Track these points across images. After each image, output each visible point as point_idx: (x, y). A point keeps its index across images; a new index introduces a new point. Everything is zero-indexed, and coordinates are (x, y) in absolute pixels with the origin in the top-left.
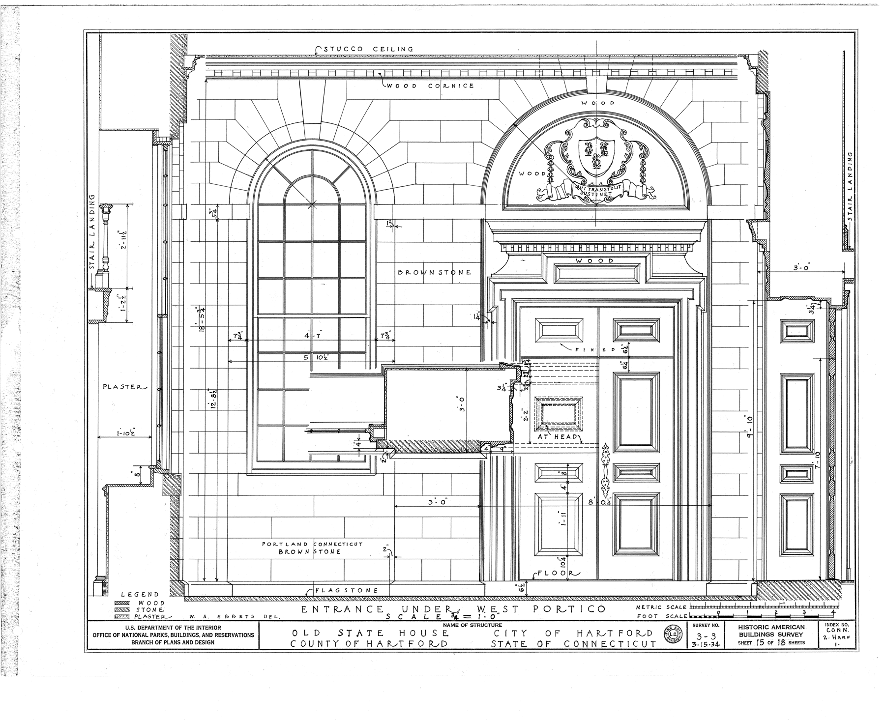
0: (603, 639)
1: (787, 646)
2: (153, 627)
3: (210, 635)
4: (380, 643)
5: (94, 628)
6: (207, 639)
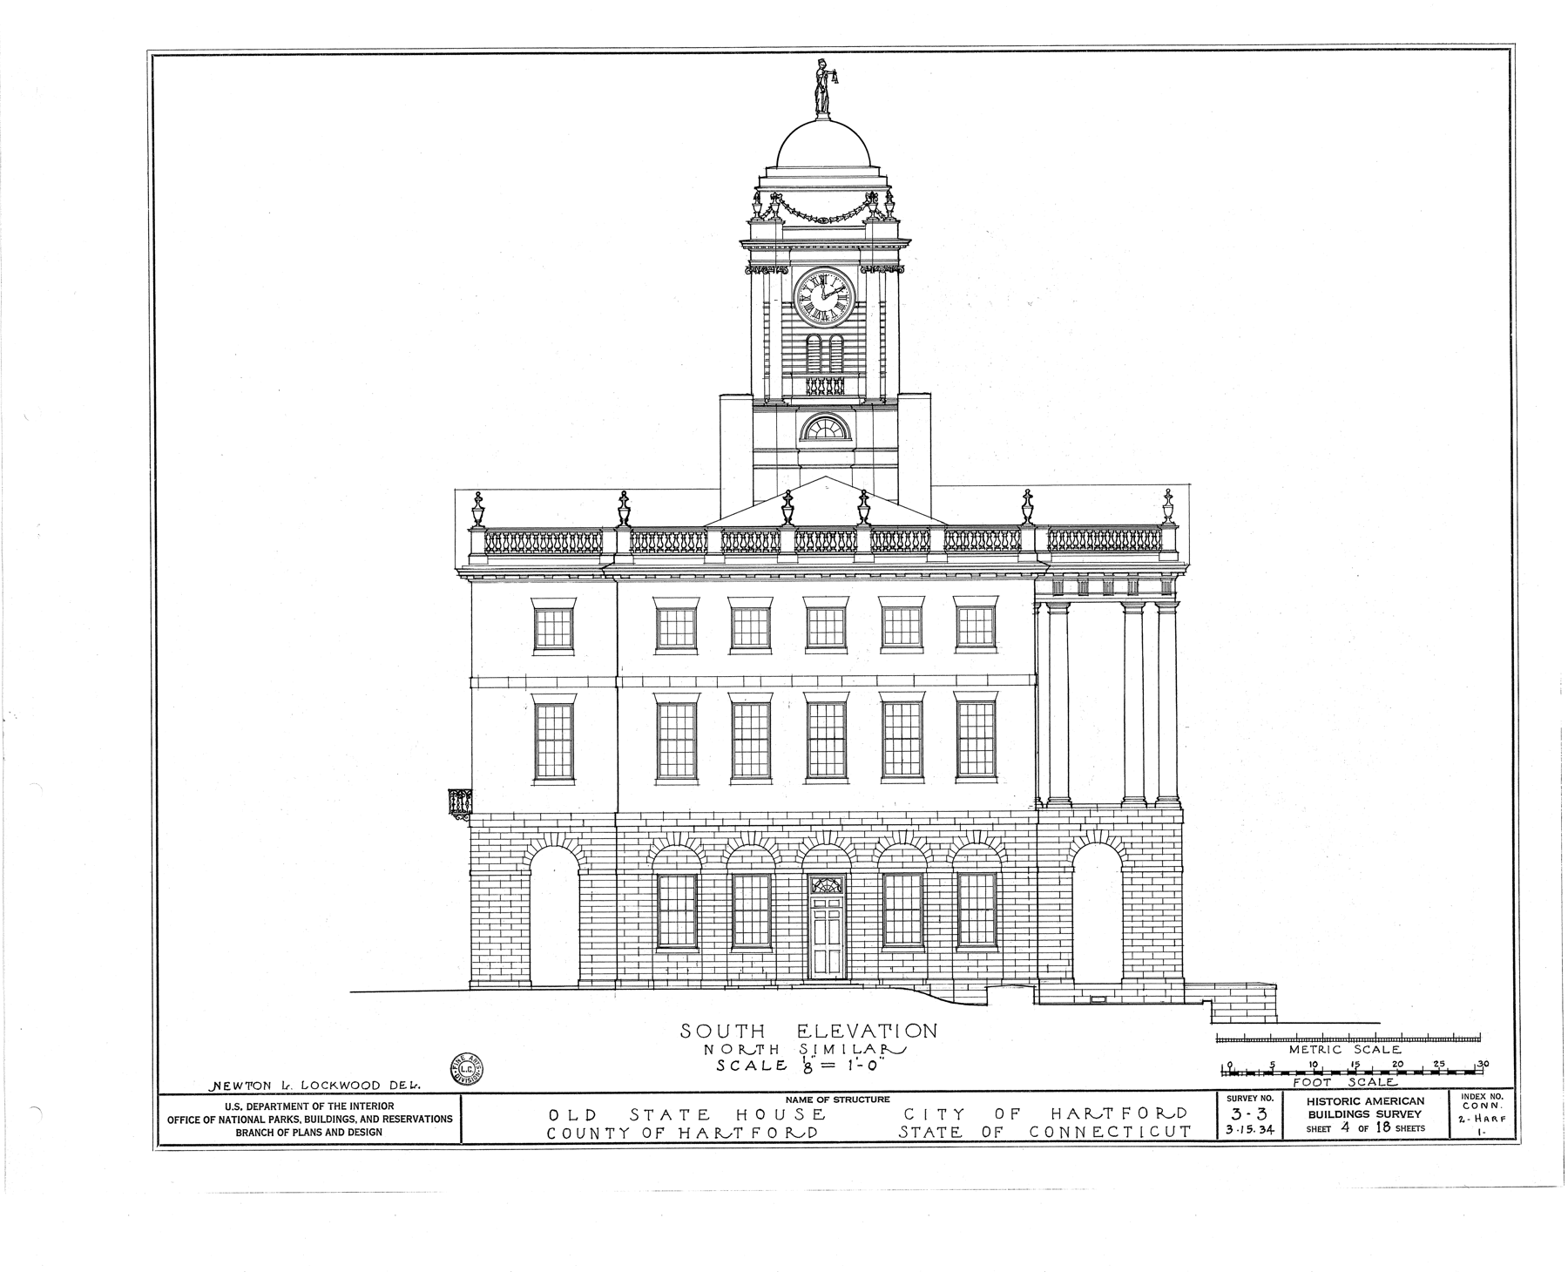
0: (1097, 1123)
1: (1393, 1134)
2: (273, 1106)
3: (374, 1119)
4: (702, 1131)
5: (170, 1107)
6: (369, 1126)
